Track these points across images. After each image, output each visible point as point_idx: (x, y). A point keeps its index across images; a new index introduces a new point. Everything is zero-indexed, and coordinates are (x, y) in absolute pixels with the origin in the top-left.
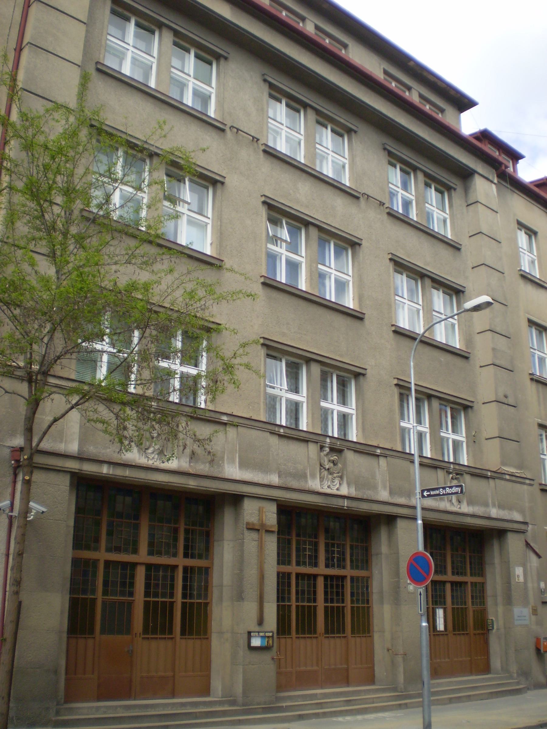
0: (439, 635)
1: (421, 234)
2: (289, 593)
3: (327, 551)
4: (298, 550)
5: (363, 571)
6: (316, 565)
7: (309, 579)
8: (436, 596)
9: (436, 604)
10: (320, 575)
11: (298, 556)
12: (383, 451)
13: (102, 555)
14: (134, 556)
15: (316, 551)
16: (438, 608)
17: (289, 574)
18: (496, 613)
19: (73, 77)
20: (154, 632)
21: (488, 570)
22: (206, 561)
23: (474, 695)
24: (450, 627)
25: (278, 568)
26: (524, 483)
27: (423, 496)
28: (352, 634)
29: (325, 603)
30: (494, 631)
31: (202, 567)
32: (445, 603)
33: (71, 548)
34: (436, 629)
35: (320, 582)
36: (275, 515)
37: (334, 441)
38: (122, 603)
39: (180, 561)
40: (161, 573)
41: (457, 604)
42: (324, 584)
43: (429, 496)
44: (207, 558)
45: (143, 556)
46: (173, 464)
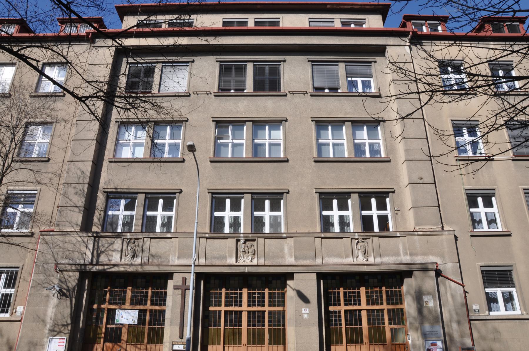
17: (340, 312)
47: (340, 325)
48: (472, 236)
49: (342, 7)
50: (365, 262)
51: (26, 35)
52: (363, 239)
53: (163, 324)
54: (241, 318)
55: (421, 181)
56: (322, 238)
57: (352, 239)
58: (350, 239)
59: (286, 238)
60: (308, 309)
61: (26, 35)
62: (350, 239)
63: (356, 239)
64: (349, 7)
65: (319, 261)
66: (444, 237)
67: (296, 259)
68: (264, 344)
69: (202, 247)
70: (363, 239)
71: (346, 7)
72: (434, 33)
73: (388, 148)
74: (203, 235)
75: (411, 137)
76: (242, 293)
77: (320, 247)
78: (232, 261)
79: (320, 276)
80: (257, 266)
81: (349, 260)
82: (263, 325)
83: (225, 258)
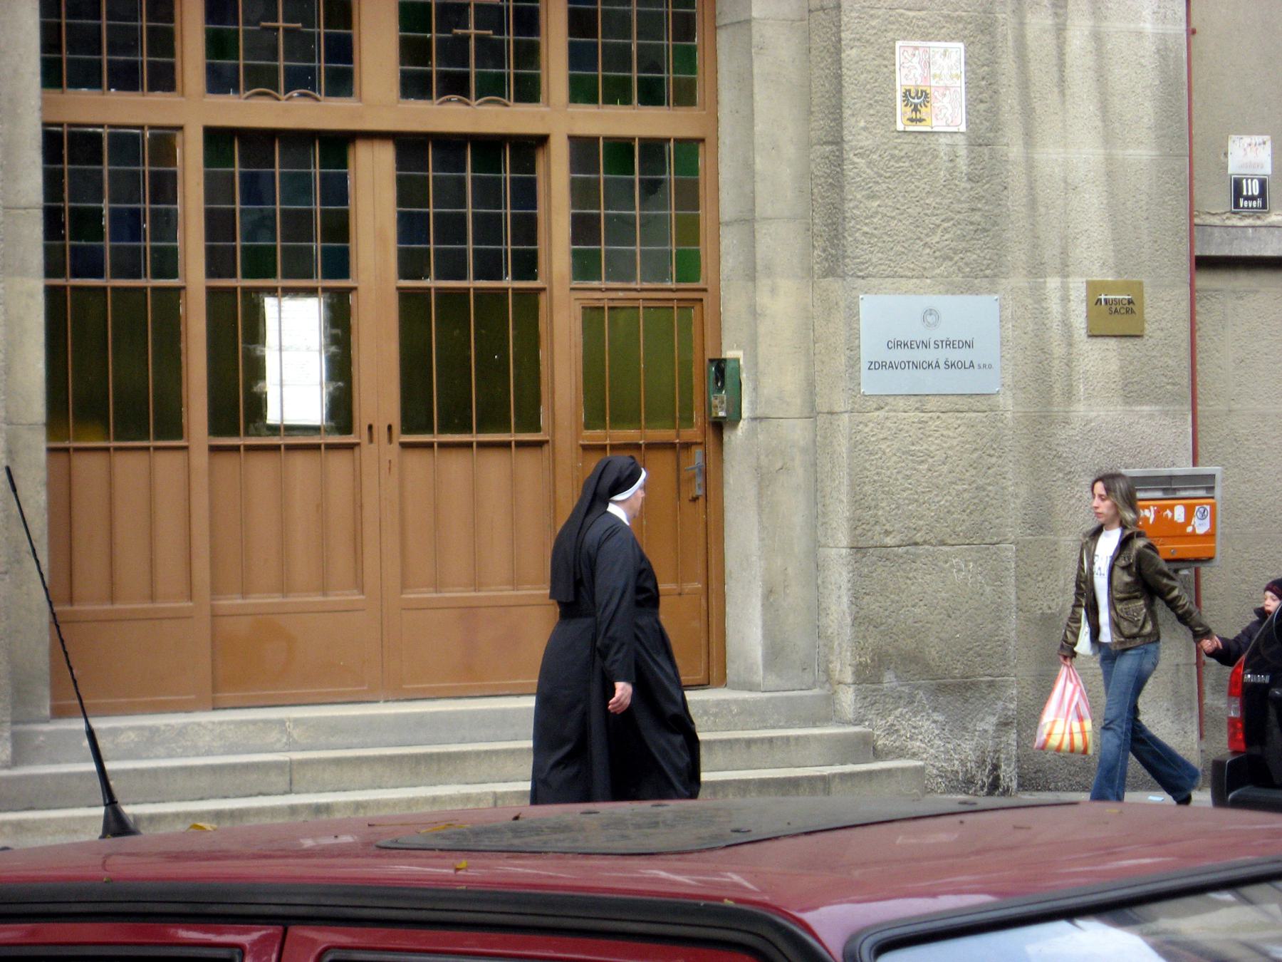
2: (167, 224)
9: (260, 264)
13: (192, 109)
14: (159, 97)
16: (272, 291)
17: (165, 140)
18: (762, 317)
20: (456, 419)
21: (724, 58)
22: (682, 112)
23: (478, 754)
25: (46, 105)
28: (215, 430)
29: (404, 275)
30: (742, 425)
32: (338, 264)
33: (37, 80)
34: (257, 405)
35: (556, 175)
39: (558, 117)
40: (508, 175)
41: (452, 267)
42: (401, 181)
44: (686, 96)
45: (378, 97)
47: (167, 263)
53: (54, 297)
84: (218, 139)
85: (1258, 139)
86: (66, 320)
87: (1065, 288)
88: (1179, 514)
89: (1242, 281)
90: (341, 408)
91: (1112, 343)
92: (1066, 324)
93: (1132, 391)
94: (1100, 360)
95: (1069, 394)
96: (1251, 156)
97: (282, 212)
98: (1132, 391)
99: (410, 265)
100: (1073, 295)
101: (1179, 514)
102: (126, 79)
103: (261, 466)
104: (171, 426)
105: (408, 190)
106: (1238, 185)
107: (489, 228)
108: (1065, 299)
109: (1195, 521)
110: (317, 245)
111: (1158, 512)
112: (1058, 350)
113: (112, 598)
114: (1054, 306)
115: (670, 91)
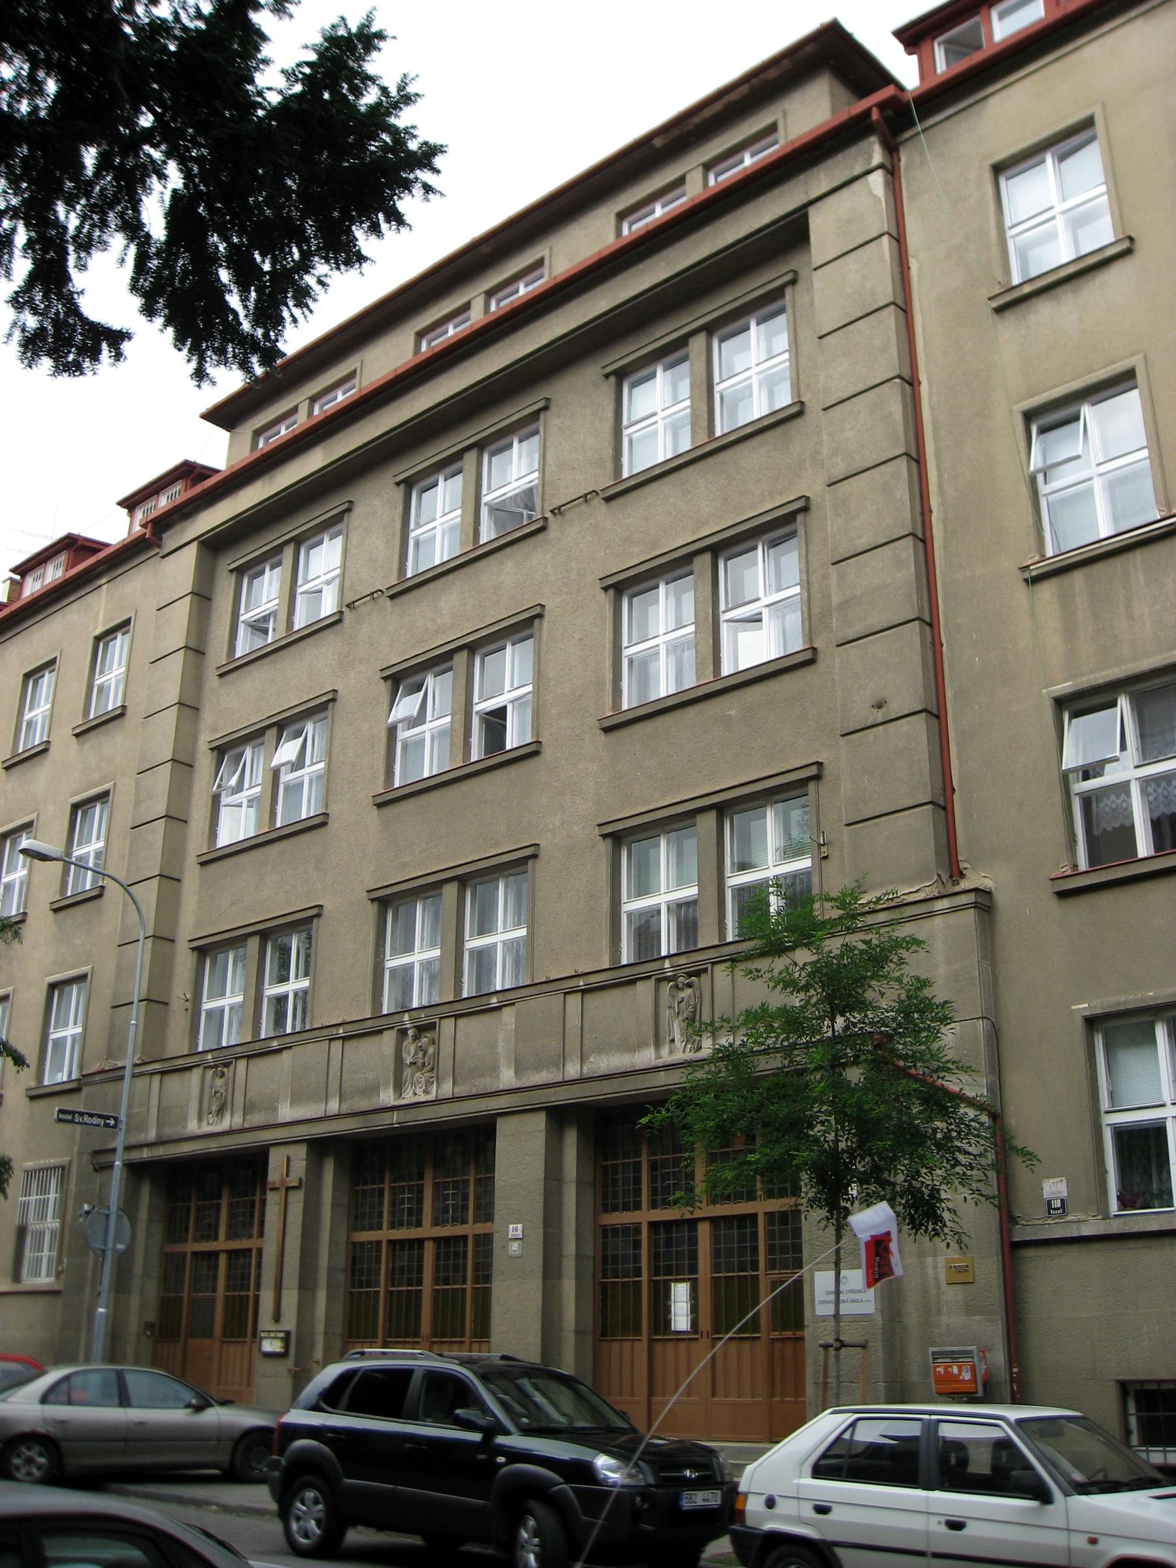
0: (678, 1340)
1: (509, 550)
3: (435, 1198)
4: (393, 1203)
5: (371, 1233)
6: (419, 1224)
7: (411, 1248)
8: (394, 1269)
10: (429, 1239)
11: (393, 1213)
12: (501, 997)
15: (420, 1201)
16: (672, 1280)
17: (637, 1228)
19: (1040, 465)
24: (705, 1324)
26: (931, 915)
27: (116, 1119)
31: (774, 1213)
32: (693, 1269)
34: (668, 1323)
36: (304, 1163)
37: (415, 1014)
38: (241, 1297)
43: (108, 1118)
46: (225, 1124)
48: (1063, 895)
49: (697, 120)
50: (690, 1056)
51: (92, 560)
52: (690, 975)
54: (696, 1244)
55: (880, 716)
56: (584, 992)
57: (659, 981)
58: (652, 982)
59: (499, 1008)
60: (520, 1226)
61: (92, 560)
62: (652, 982)
63: (669, 979)
64: (717, 107)
65: (573, 1070)
66: (938, 921)
67: (519, 1070)
68: (640, 1335)
69: (573, 1019)
70: (690, 975)
71: (707, 113)
72: (976, 58)
73: (816, 610)
74: (572, 983)
75: (862, 543)
76: (422, 1185)
77: (578, 1022)
78: (387, 1097)
79: (560, 1116)
80: (582, 1080)
81: (646, 1057)
82: (214, 1290)
83: (375, 1090)
84: (653, 1225)
85: (1058, 1179)
86: (376, 1311)
87: (935, 1262)
88: (955, 1370)
89: (1053, 1251)
90: (694, 1323)
91: (960, 1286)
92: (936, 1279)
93: (970, 1309)
94: (954, 1295)
95: (939, 1312)
96: (1054, 1189)
97: (672, 1251)
98: (970, 1309)
99: (716, 1267)
100: (939, 1265)
101: (955, 1370)
102: (626, 1208)
103: (670, 1347)
104: (637, 1330)
105: (716, 1240)
106: (1049, 1203)
107: (742, 1250)
108: (935, 1267)
109: (964, 1373)
110: (686, 1262)
111: (946, 1368)
112: (933, 1291)
113: (621, 1395)
114: (930, 1271)
115: (481, 1228)
